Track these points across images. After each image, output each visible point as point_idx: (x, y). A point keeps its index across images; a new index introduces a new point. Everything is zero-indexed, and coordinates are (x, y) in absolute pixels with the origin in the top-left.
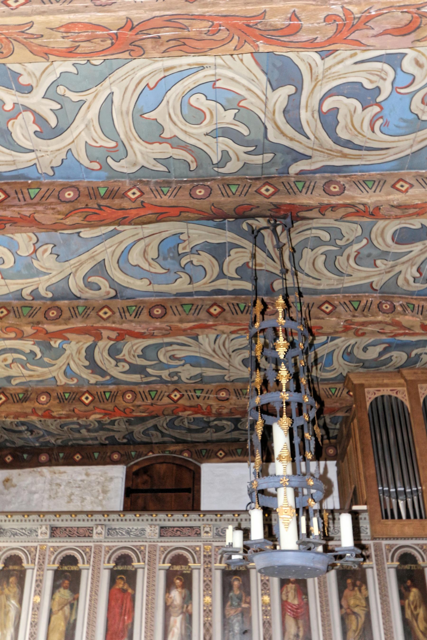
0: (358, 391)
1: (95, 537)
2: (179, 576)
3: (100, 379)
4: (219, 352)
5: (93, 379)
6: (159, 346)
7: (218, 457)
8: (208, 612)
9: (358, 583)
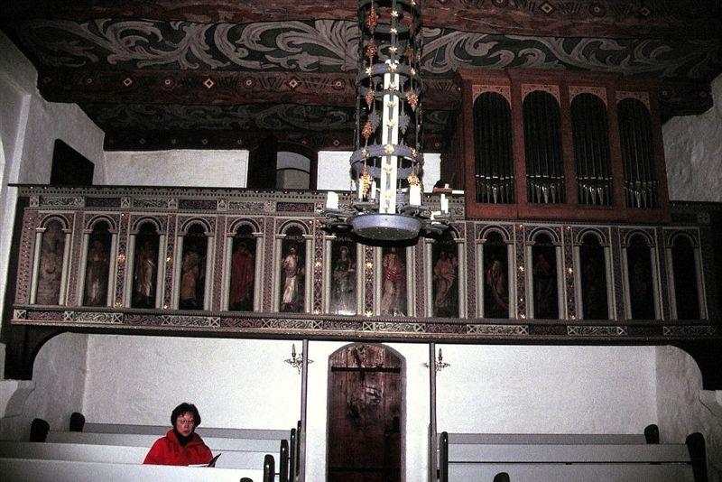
0: (464, 85)
1: (218, 209)
2: (294, 244)
3: (221, 64)
4: (335, 41)
5: (214, 64)
6: (278, 32)
7: (334, 145)
8: (318, 275)
9: (450, 255)
